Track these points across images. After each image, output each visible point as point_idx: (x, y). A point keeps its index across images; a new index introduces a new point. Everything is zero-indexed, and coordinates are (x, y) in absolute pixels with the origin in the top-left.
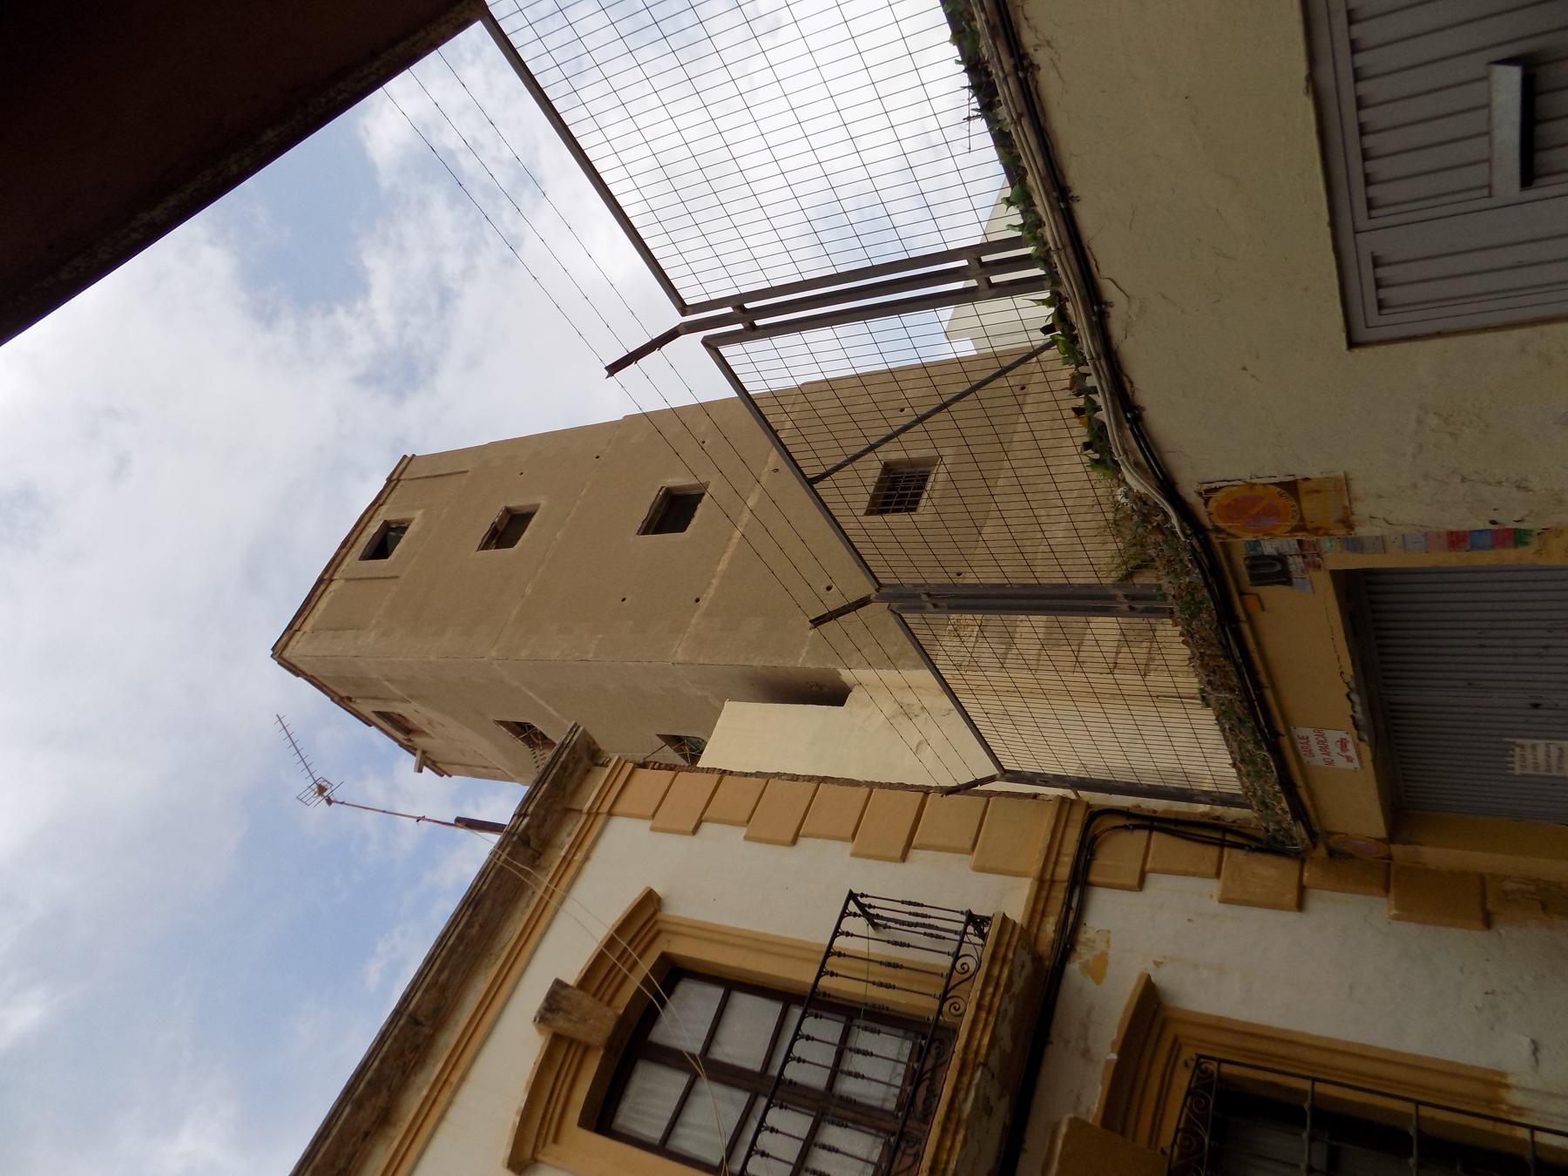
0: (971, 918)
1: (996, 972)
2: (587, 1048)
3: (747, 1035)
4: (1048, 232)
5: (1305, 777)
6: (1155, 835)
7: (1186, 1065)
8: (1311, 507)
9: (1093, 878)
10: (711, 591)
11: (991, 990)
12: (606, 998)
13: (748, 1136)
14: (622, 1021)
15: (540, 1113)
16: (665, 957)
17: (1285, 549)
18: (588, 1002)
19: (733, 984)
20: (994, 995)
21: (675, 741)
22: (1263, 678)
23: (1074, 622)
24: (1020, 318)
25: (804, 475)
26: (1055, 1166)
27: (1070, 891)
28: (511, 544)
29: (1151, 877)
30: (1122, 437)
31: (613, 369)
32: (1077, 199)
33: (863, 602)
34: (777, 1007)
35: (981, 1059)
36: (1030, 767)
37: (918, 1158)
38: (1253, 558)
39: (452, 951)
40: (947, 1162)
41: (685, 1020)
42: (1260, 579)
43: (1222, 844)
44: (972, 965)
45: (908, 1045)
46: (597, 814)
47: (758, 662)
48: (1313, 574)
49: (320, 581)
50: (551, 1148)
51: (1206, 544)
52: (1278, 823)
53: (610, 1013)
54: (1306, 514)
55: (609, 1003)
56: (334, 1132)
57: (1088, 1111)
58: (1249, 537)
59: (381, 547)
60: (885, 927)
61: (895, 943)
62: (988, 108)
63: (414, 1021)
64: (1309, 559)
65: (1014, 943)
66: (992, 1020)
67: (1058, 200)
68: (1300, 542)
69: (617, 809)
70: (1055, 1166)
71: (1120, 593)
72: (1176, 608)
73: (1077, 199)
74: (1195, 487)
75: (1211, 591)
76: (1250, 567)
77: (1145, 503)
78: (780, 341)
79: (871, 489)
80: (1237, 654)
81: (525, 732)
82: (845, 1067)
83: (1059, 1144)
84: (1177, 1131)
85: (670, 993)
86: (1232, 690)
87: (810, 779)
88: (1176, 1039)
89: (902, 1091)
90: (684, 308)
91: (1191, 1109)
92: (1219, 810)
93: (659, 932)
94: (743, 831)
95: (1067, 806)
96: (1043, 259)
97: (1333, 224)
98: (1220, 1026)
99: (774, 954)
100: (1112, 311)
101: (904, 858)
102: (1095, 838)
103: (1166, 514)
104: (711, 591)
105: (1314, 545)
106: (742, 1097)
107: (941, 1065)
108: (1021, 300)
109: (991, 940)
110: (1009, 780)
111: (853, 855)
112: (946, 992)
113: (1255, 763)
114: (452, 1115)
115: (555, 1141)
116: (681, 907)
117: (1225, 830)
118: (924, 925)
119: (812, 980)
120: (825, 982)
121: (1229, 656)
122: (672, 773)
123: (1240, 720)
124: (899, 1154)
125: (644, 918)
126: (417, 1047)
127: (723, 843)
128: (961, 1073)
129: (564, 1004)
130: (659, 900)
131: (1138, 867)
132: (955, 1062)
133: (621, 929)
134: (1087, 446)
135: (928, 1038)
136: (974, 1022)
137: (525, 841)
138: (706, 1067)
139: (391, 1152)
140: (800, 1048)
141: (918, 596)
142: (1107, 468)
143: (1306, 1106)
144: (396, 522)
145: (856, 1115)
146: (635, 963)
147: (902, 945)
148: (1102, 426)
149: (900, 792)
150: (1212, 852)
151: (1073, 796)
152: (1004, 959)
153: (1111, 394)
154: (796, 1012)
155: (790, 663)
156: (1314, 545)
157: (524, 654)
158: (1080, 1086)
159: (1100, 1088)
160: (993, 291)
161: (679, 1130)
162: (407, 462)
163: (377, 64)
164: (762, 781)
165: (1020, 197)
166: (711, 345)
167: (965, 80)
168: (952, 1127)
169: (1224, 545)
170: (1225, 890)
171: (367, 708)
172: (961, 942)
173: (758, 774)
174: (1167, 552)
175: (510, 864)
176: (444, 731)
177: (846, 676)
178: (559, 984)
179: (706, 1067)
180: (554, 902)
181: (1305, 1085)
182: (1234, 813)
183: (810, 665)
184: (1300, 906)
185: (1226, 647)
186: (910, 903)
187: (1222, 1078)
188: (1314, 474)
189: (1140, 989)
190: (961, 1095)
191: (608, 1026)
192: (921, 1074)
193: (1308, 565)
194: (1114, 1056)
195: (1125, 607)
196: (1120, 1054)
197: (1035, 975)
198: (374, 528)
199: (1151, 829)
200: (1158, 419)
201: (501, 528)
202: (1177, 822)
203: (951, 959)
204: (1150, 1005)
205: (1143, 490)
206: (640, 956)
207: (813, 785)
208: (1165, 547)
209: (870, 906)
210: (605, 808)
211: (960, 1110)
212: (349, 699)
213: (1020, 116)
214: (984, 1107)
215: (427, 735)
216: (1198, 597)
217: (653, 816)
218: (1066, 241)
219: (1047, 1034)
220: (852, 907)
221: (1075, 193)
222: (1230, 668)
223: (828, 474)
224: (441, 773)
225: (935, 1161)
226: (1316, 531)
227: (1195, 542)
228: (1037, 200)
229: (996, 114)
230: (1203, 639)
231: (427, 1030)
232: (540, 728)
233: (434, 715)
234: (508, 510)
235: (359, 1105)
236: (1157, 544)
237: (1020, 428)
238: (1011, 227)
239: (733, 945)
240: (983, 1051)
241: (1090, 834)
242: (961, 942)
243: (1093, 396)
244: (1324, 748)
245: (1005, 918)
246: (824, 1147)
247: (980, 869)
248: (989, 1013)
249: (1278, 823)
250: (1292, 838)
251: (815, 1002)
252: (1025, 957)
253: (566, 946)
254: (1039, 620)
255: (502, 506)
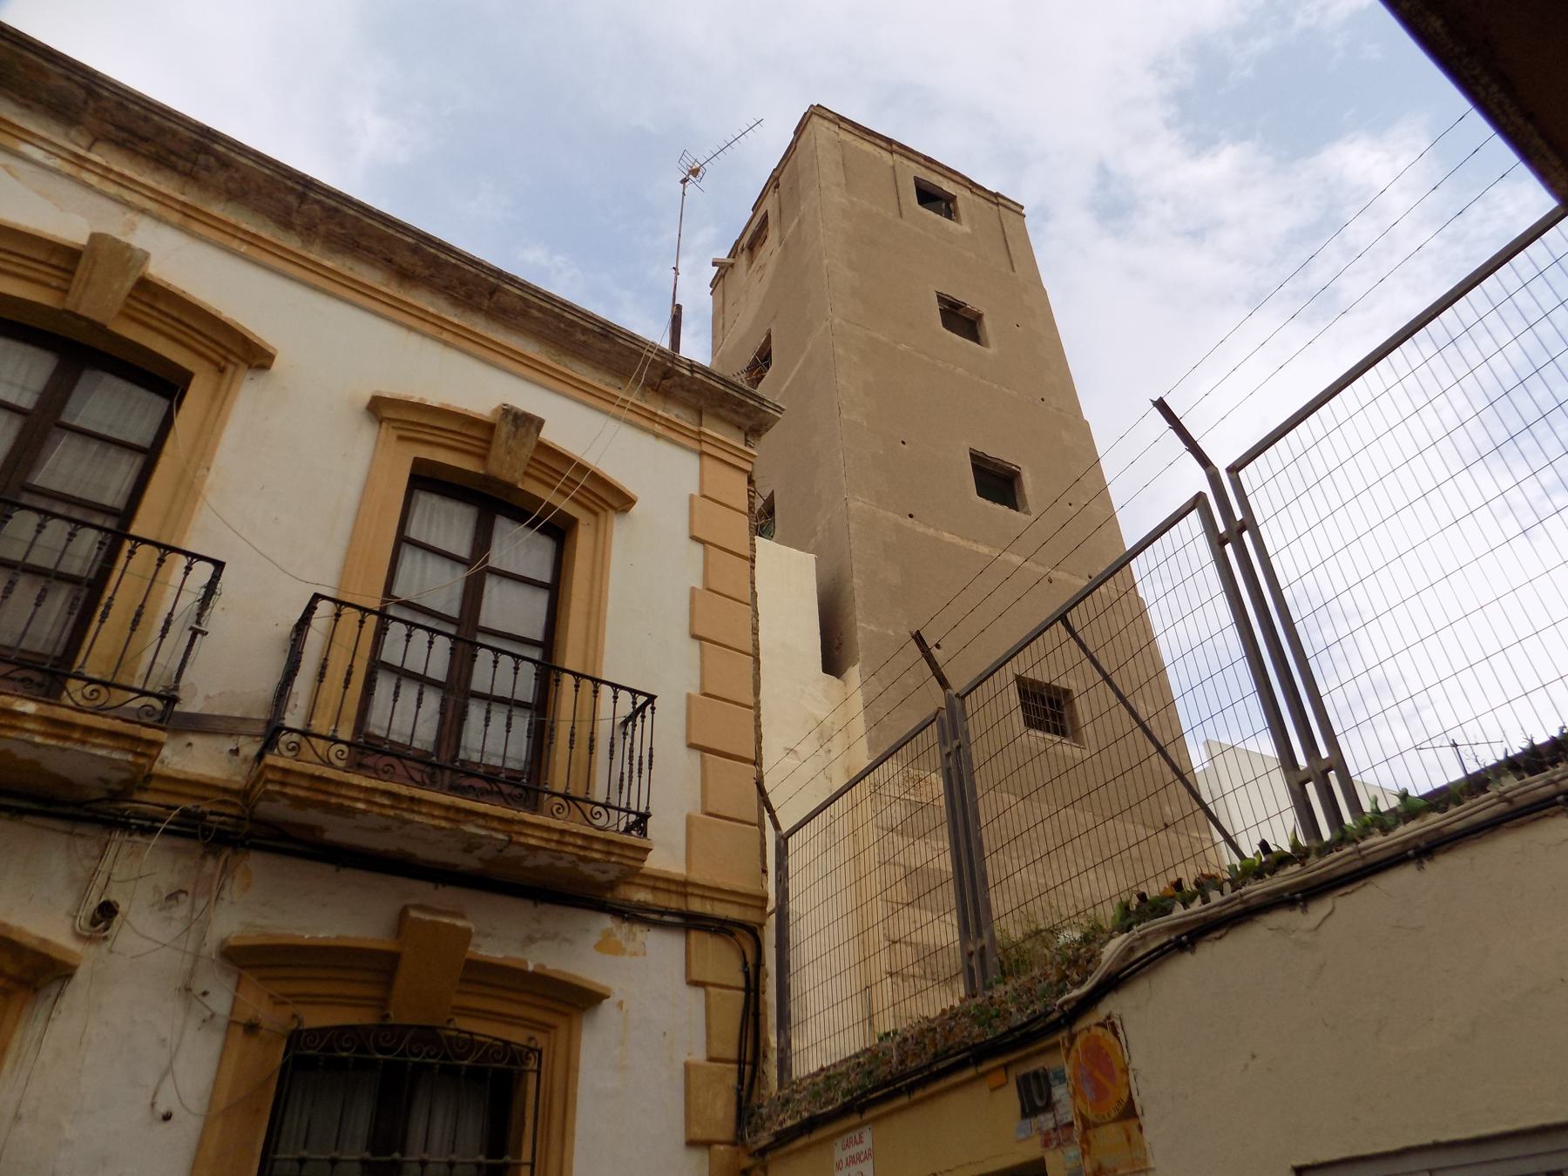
0: (643, 818)
1: (596, 846)
2: (483, 458)
3: (511, 610)
4: (1376, 839)
5: (820, 1142)
6: (742, 994)
7: (531, 1039)
8: (1111, 1134)
9: (693, 935)
10: (921, 529)
11: (579, 842)
12: (531, 470)
13: (421, 620)
14: (512, 488)
15: (423, 421)
16: (573, 522)
17: (1061, 1110)
18: (526, 452)
19: (556, 590)
20: (575, 846)
21: (769, 509)
22: (918, 1094)
23: (948, 895)
24: (1261, 816)
25: (1069, 610)
26: (428, 917)
27: (679, 913)
28: (946, 324)
29: (701, 992)
30: (1158, 933)
31: (1161, 405)
32: (1421, 868)
33: (943, 682)
34: (538, 636)
35: (515, 838)
36: (793, 863)
37: (421, 785)
38: (1046, 1077)
39: (560, 318)
40: (420, 813)
41: (519, 548)
42: (1024, 1084)
43: (741, 1061)
44: (601, 822)
45: (518, 766)
46: (700, 441)
47: (857, 582)
48: (1038, 1139)
49: (890, 141)
50: (393, 434)
51: (1055, 1027)
52: (770, 1118)
53: (518, 475)
54: (1103, 1130)
55: (526, 474)
56: (390, 231)
57: (478, 946)
58: (1068, 1071)
59: (929, 196)
60: (625, 734)
61: (612, 745)
62: (1512, 765)
63: (493, 291)
64: (1053, 1135)
65: (625, 861)
66: (553, 846)
67: (1416, 848)
68: (1071, 1124)
69: (706, 460)
70: (428, 917)
71: (986, 941)
72: (979, 1000)
73: (1421, 868)
74: (1116, 1012)
75: (1005, 1035)
76: (1036, 1075)
77: (1089, 961)
78: (1212, 572)
79: (1055, 683)
80: (941, 1065)
81: (763, 360)
82: (495, 707)
83: (446, 920)
84: (471, 1034)
85: (542, 531)
86: (902, 1062)
87: (756, 647)
88: (554, 1027)
89: (478, 764)
90: (1234, 470)
91: (491, 1046)
92: (773, 1057)
93: (596, 514)
94: (699, 585)
95: (759, 904)
96: (1343, 837)
97: (1436, 1147)
98: (570, 1069)
99: (588, 628)
100: (1297, 913)
101: (691, 746)
102: (732, 934)
103: (1082, 982)
104: (921, 529)
105: (1069, 1140)
106: (454, 610)
107: (508, 800)
108: (1291, 818)
109: (626, 838)
110: (777, 844)
111: (689, 696)
112: (573, 799)
113: (828, 1089)
114: (414, 341)
115: (400, 438)
116: (621, 531)
117: (755, 1065)
118: (631, 772)
119: (568, 666)
120: (568, 680)
121: (937, 1057)
122: (746, 510)
123: (870, 1073)
124: (421, 767)
125: (609, 499)
126: (470, 297)
127: (684, 567)
128: (500, 819)
129: (522, 431)
130: (626, 511)
131: (709, 979)
132: (509, 813)
133: (597, 478)
134: (1142, 897)
135: (527, 784)
136: (549, 829)
137: (668, 374)
138: (478, 574)
139: (376, 286)
140: (506, 662)
141: (956, 737)
142: (1122, 919)
143: (508, 1158)
144: (956, 208)
145: (452, 724)
146: (566, 495)
147: (612, 752)
148: (1167, 911)
149: (753, 736)
150: (732, 1052)
151: (769, 909)
152: (609, 853)
153: (1204, 919)
154: (536, 654)
155: (859, 614)
156: (1069, 1140)
157: (840, 351)
158: (502, 936)
159: (499, 955)
160: (1296, 787)
161: (419, 554)
162: (1017, 210)
163: (1520, 121)
164: (748, 599)
165: (1410, 808)
166: (1198, 501)
167: (1541, 739)
168: (451, 815)
169: (1056, 1046)
170: (696, 1066)
171: (770, 205)
172: (620, 810)
173: (754, 594)
174: (1040, 987)
175: (645, 363)
176: (754, 283)
177: (854, 673)
178: (539, 423)
179: (478, 574)
180: (614, 409)
181: (526, 1156)
182: (772, 1072)
183: (860, 635)
184: (692, 1143)
185: (946, 1054)
186: (651, 756)
187: (523, 1073)
188: (1148, 1136)
189: (594, 988)
190: (481, 822)
191: (506, 475)
192: (494, 781)
193: (1047, 1133)
194: (531, 968)
195: (971, 947)
196: (534, 974)
197: (592, 886)
198: (948, 187)
199: (747, 990)
200: (1185, 967)
201: (960, 312)
202: (757, 1015)
203: (603, 801)
204: (581, 1000)
205: (1104, 957)
206: (573, 499)
207: (750, 649)
208: (1044, 984)
209: (643, 717)
210: (706, 448)
211: (465, 822)
212: (777, 186)
213: (1510, 801)
214: (471, 844)
215: (750, 265)
216: (996, 1022)
217: (704, 496)
218: (1371, 859)
219: (543, 901)
220: (641, 700)
221: (1427, 864)
222: (925, 1059)
223: (1074, 634)
224: (714, 284)
225: (420, 801)
226: (1085, 1140)
227: (1055, 1016)
228: (1412, 825)
229: (1507, 775)
230: (951, 1030)
231: (486, 304)
232: (768, 374)
233: (770, 269)
234: (979, 316)
235: (415, 250)
236: (1045, 975)
237: (1140, 828)
238: (1375, 801)
239: (592, 587)
240: (523, 840)
241: (734, 929)
242: (620, 810)
243: (1199, 900)
244: (853, 1160)
245: (648, 850)
246: (421, 694)
247: (690, 821)
248: (558, 842)
249: (770, 1118)
250: (756, 1132)
251: (548, 672)
252: (613, 873)
253: (576, 427)
254: (945, 863)
255: (983, 310)
